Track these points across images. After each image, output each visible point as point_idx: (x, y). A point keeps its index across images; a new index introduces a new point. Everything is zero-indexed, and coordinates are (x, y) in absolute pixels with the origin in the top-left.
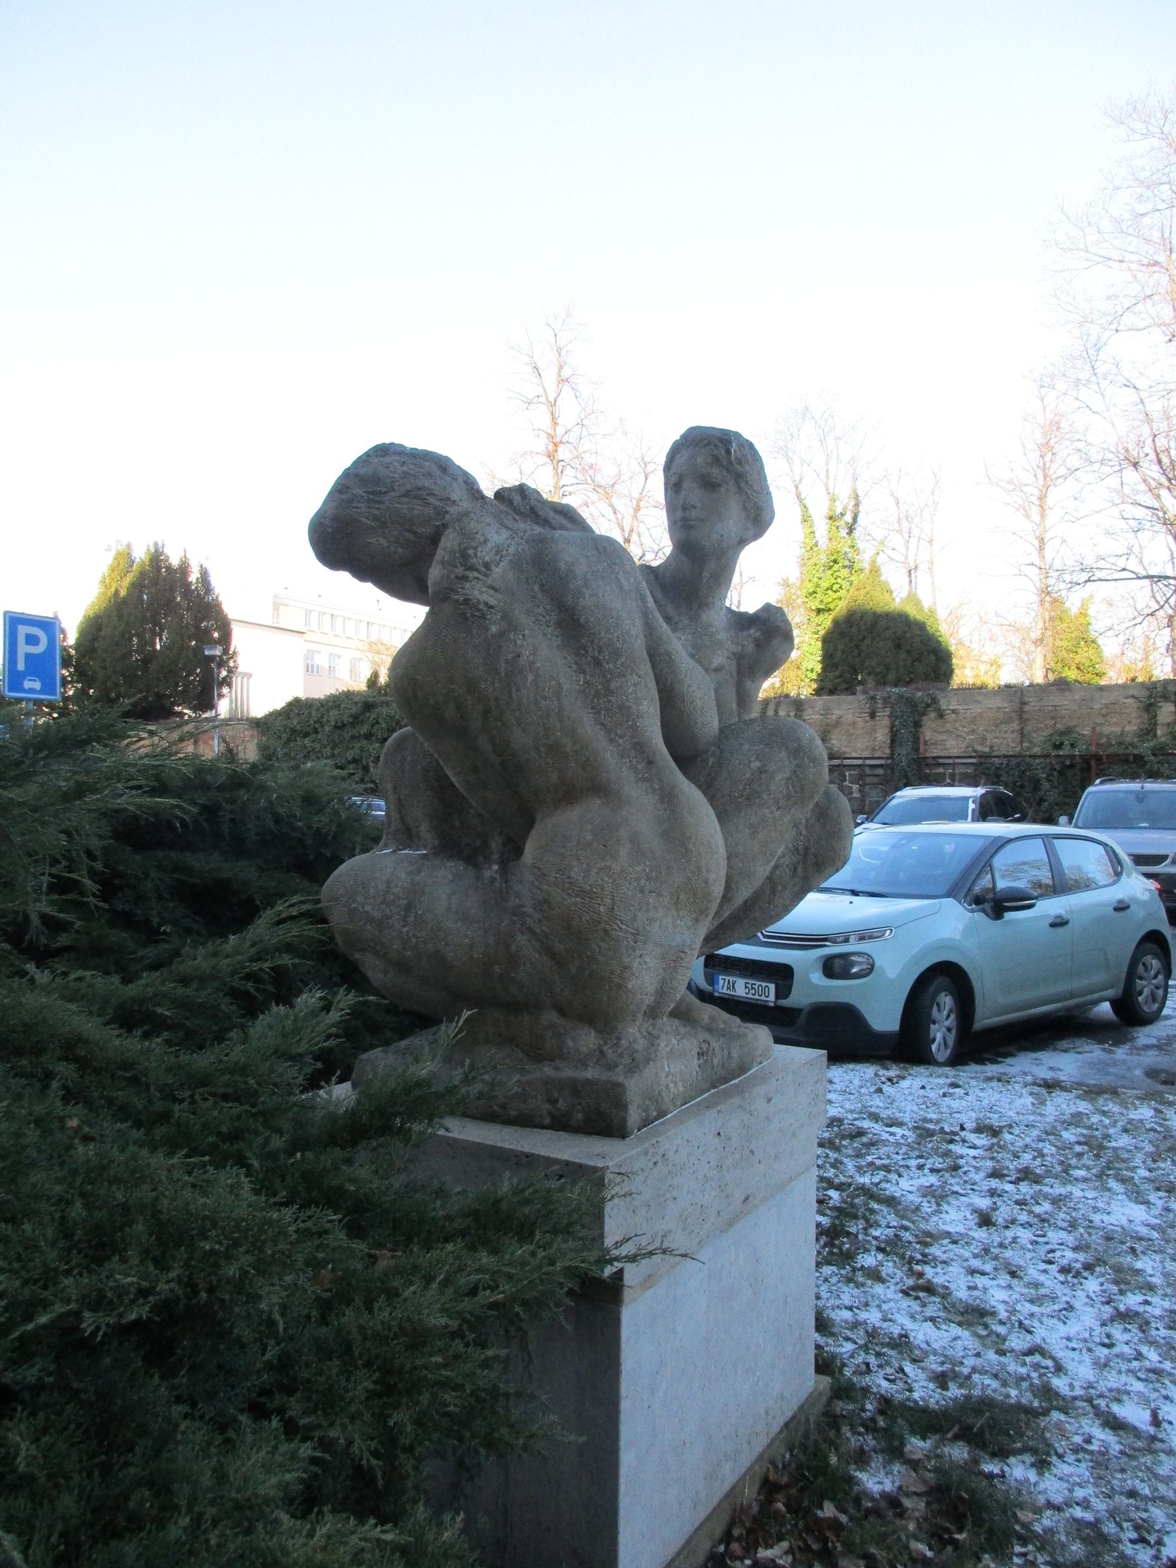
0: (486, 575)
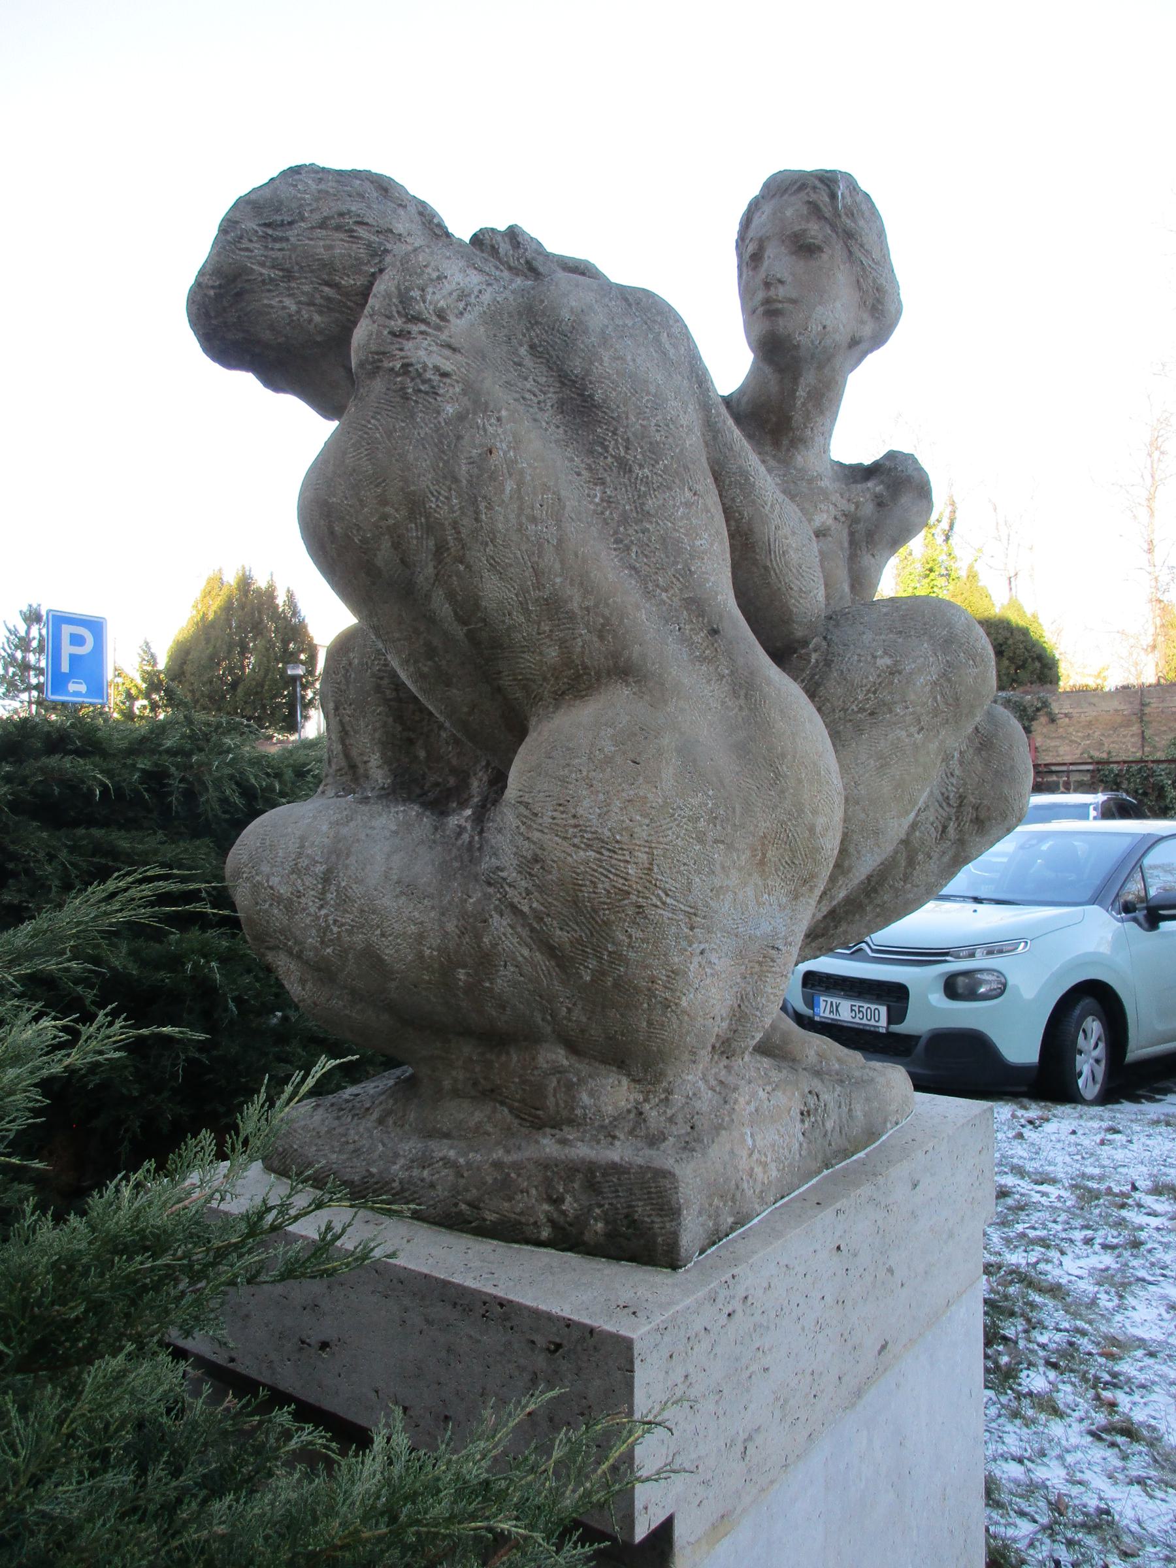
0: (439, 328)
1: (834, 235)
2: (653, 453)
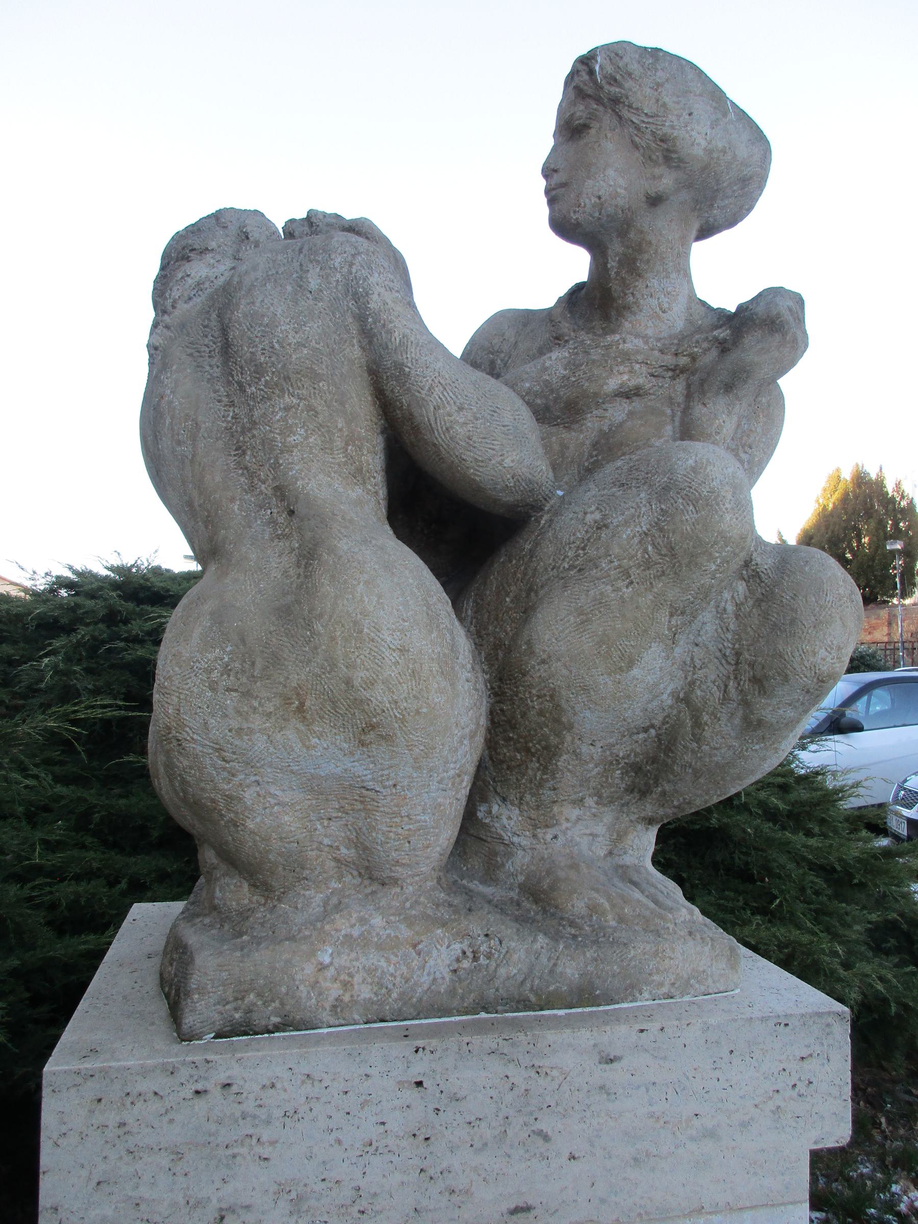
1: (601, 108)
2: (258, 373)
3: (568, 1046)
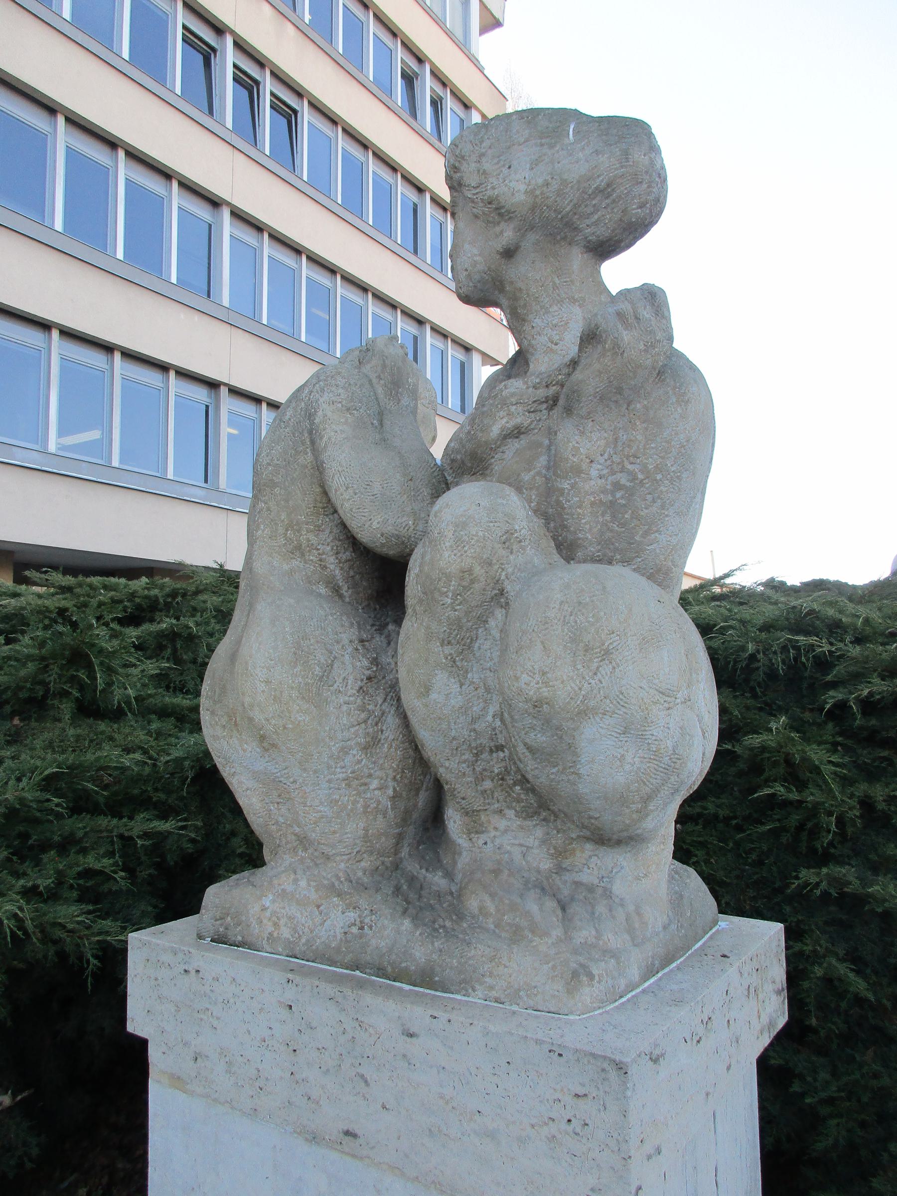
3: (385, 1011)
